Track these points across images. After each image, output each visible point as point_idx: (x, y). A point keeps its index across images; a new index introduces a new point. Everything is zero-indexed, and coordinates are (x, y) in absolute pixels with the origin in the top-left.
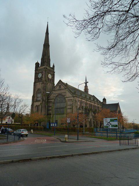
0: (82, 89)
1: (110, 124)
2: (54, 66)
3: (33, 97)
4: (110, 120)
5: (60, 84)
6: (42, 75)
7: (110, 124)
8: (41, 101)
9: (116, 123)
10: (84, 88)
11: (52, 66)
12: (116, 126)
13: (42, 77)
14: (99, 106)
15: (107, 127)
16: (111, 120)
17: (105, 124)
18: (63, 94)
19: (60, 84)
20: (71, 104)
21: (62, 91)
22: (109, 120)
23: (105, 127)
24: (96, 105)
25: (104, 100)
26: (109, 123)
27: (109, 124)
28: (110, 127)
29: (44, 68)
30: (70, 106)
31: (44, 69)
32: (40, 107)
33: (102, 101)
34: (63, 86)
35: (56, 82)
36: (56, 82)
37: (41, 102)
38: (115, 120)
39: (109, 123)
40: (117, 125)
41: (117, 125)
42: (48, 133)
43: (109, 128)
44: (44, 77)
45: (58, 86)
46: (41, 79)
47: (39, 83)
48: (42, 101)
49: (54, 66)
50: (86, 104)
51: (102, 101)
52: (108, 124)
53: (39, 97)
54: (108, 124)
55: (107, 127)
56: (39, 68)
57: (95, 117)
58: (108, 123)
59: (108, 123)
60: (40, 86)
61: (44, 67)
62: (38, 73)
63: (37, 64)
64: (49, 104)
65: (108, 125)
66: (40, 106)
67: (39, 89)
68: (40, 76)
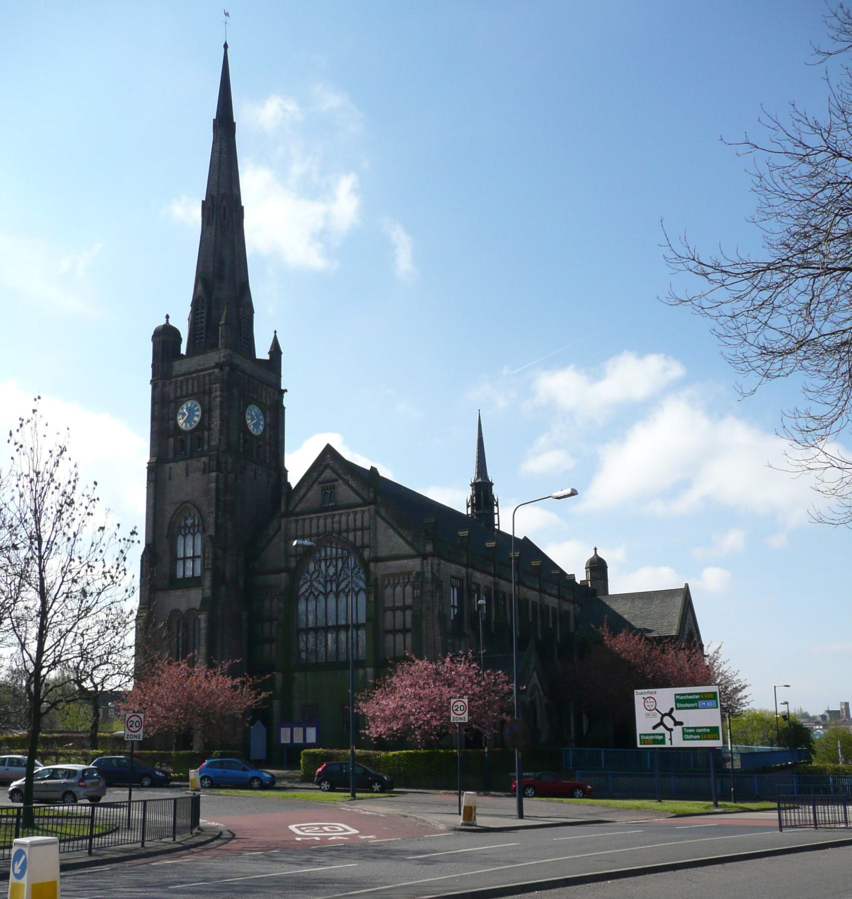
0: (456, 497)
1: (677, 723)
2: (276, 351)
3: (150, 559)
4: (677, 701)
5: (328, 474)
6: (207, 412)
7: (677, 723)
8: (207, 583)
9: (710, 717)
10: (468, 493)
11: (262, 352)
12: (713, 732)
13: (209, 429)
14: (566, 606)
15: (655, 742)
16: (682, 702)
17: (644, 724)
18: (351, 537)
19: (328, 474)
20: (409, 601)
21: (346, 519)
22: (665, 697)
23: (643, 742)
24: (552, 602)
25: (598, 567)
26: (668, 721)
27: (668, 721)
28: (677, 740)
29: (220, 366)
30: (399, 614)
31: (214, 378)
32: (203, 625)
33: (581, 575)
34: (346, 483)
35: (297, 464)
36: (297, 464)
37: (208, 592)
38: (705, 697)
39: (669, 714)
40: (717, 728)
41: (714, 730)
42: (326, 877)
43: (668, 744)
44: (216, 423)
45: (316, 487)
46: (200, 439)
47: (182, 465)
48: (214, 586)
49: (276, 351)
50: (496, 597)
51: (581, 575)
52: (661, 723)
53: (185, 559)
54: (661, 723)
55: (655, 742)
56: (179, 367)
57: (558, 678)
58: (663, 716)
59: (663, 716)
60: (192, 482)
61: (214, 357)
62: (178, 402)
63: (165, 337)
64: (312, 633)
65: (661, 729)
66: (203, 617)
67: (184, 507)
68: (187, 417)
